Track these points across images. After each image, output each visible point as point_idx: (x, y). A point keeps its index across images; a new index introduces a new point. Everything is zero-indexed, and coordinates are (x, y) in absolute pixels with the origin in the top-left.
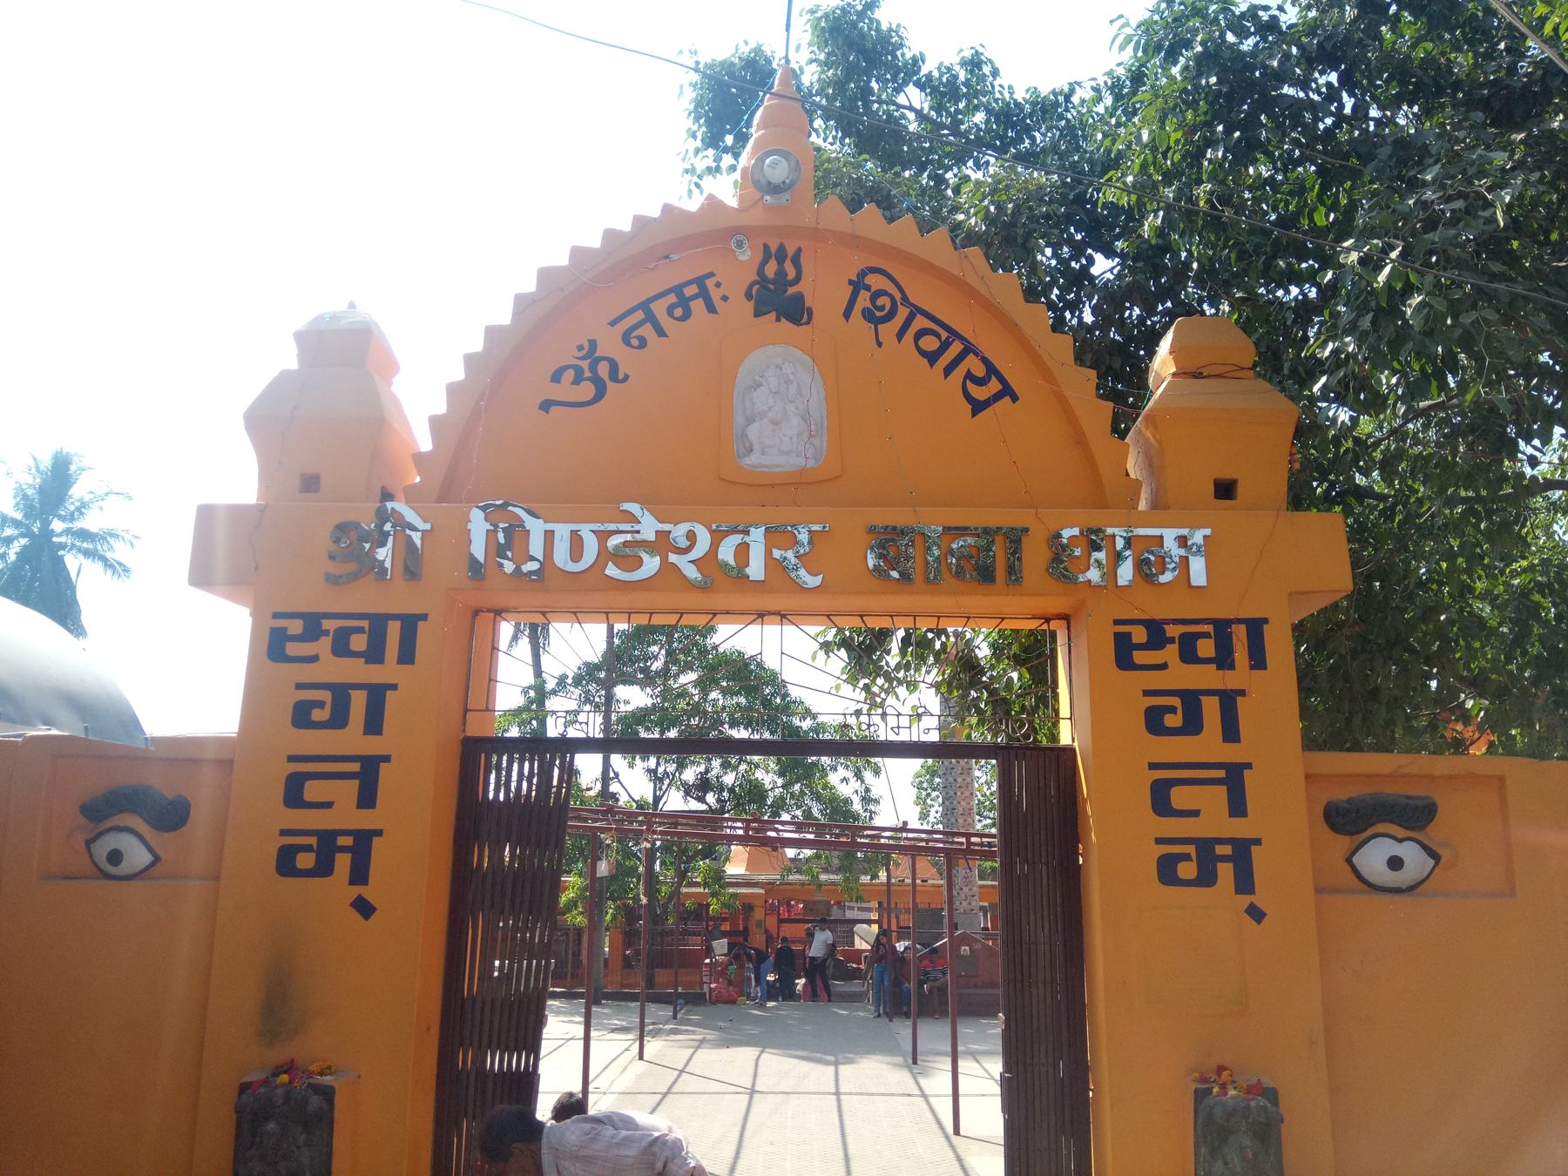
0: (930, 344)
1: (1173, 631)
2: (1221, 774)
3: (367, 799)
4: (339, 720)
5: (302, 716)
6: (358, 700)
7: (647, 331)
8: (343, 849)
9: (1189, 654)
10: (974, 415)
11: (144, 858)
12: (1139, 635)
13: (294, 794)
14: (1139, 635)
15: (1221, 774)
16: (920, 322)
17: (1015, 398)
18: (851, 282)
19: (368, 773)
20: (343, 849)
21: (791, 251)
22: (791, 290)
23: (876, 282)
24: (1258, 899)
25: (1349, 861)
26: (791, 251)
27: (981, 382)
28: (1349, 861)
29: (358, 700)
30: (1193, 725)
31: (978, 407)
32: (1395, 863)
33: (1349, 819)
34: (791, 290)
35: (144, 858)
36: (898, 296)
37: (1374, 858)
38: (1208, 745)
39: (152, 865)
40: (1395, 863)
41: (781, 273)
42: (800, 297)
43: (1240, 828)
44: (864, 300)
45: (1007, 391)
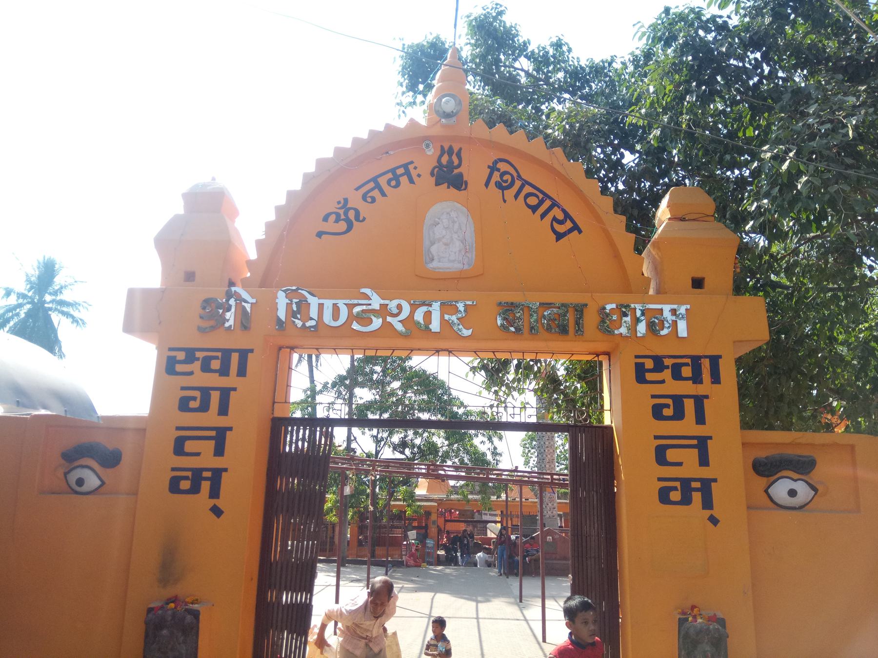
0: (533, 201)
1: (668, 362)
2: (695, 442)
3: (219, 451)
4: (204, 407)
5: (184, 405)
6: (215, 397)
7: (376, 193)
8: (206, 479)
9: (677, 375)
12: (649, 364)
13: (179, 448)
14: (649, 364)
15: (695, 442)
16: (528, 189)
17: (580, 232)
19: (220, 438)
20: (206, 479)
21: (456, 151)
22: (456, 171)
25: (766, 491)
27: (561, 222)
28: (766, 491)
29: (215, 397)
30: (679, 415)
31: (559, 236)
32: (792, 493)
33: (767, 468)
34: (456, 171)
36: (515, 175)
38: (688, 426)
39: (100, 486)
40: (792, 493)
41: (450, 162)
42: (461, 175)
44: (496, 177)
45: (576, 228)
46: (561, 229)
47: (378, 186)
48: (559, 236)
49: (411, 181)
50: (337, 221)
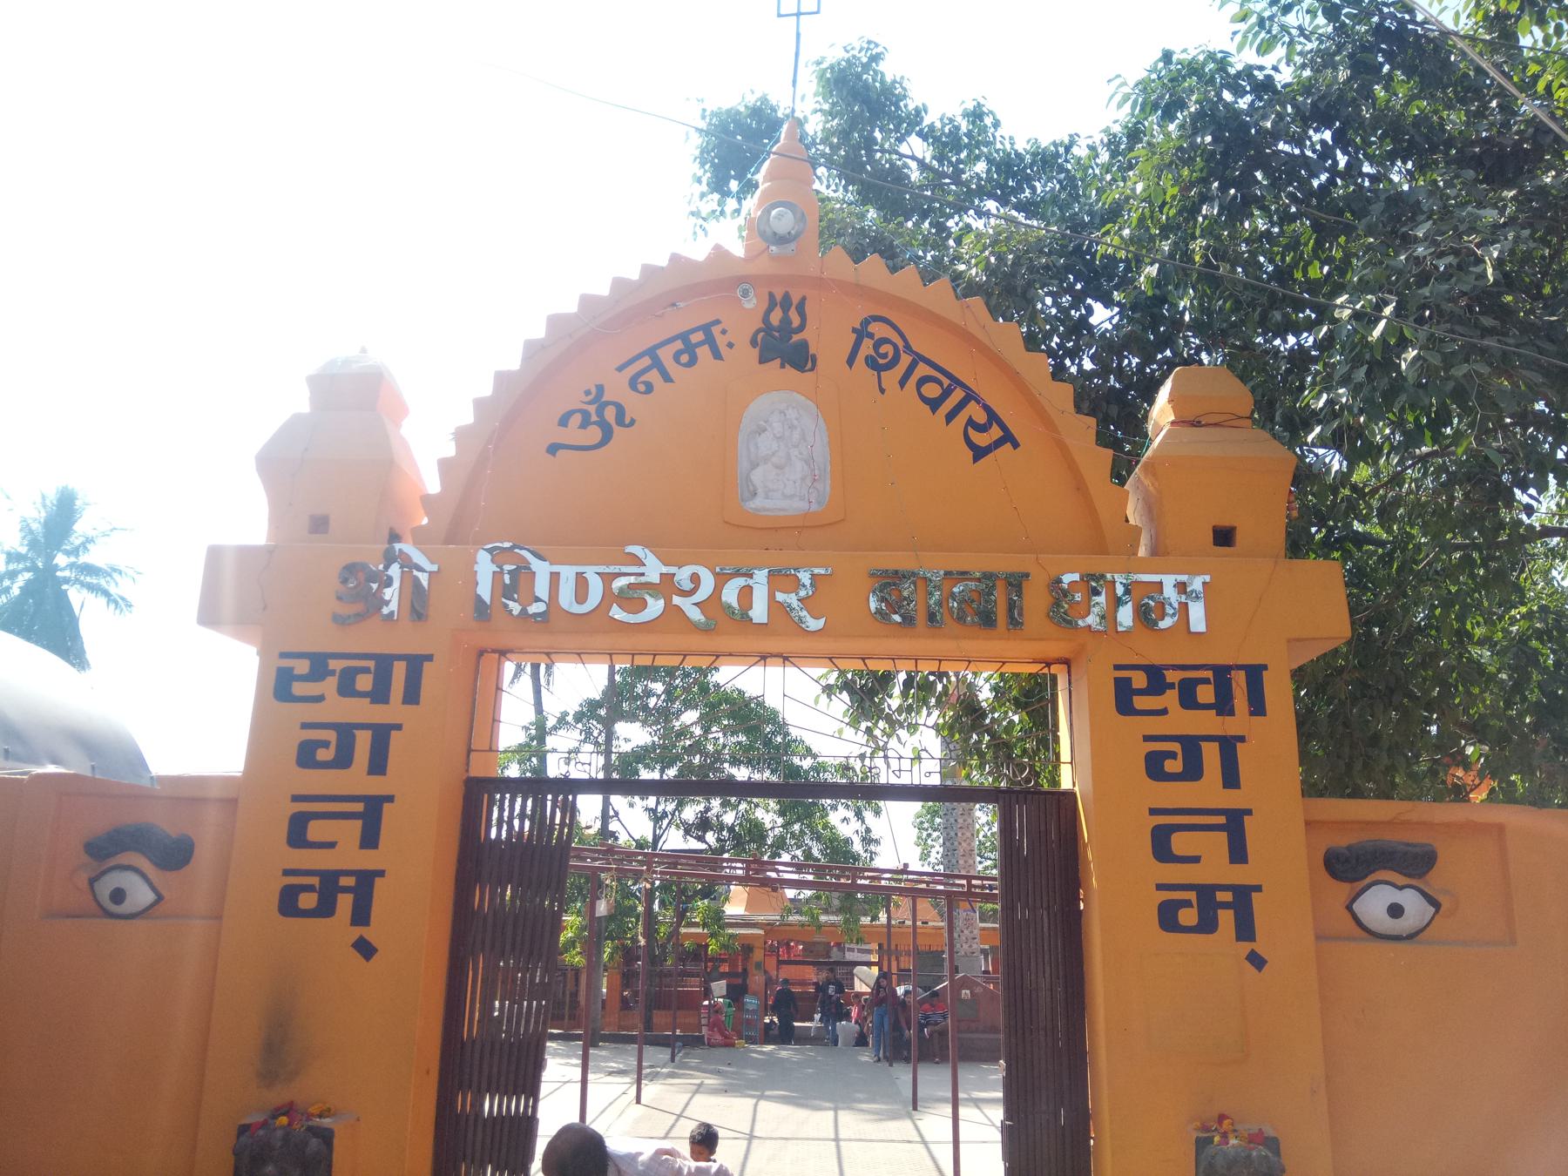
0: (932, 391)
1: (1172, 677)
2: (1222, 820)
6: (363, 740)
7: (654, 376)
8: (346, 890)
9: (1188, 700)
10: (975, 460)
11: (147, 896)
14: (1139, 680)
15: (1222, 820)
16: (922, 370)
17: (1016, 445)
18: (854, 330)
20: (346, 890)
21: (795, 301)
22: (796, 338)
23: (878, 330)
24: (1260, 946)
26: (795, 301)
27: (982, 429)
28: (1349, 908)
29: (363, 740)
31: (979, 453)
32: (1396, 911)
33: (1349, 866)
34: (796, 338)
35: (147, 896)
36: (901, 344)
37: (1374, 904)
38: (1208, 791)
40: (1396, 911)
41: (786, 321)
42: (804, 345)
43: (367, 860)
44: (867, 348)
45: (1008, 438)
46: (981, 439)
47: (657, 364)
48: (979, 453)
49: (717, 355)
50: (584, 425)
